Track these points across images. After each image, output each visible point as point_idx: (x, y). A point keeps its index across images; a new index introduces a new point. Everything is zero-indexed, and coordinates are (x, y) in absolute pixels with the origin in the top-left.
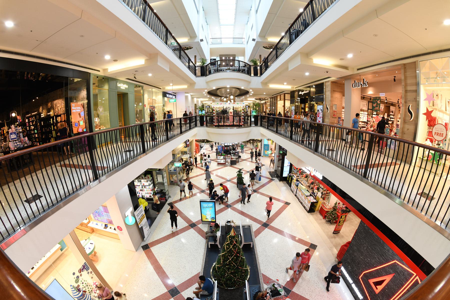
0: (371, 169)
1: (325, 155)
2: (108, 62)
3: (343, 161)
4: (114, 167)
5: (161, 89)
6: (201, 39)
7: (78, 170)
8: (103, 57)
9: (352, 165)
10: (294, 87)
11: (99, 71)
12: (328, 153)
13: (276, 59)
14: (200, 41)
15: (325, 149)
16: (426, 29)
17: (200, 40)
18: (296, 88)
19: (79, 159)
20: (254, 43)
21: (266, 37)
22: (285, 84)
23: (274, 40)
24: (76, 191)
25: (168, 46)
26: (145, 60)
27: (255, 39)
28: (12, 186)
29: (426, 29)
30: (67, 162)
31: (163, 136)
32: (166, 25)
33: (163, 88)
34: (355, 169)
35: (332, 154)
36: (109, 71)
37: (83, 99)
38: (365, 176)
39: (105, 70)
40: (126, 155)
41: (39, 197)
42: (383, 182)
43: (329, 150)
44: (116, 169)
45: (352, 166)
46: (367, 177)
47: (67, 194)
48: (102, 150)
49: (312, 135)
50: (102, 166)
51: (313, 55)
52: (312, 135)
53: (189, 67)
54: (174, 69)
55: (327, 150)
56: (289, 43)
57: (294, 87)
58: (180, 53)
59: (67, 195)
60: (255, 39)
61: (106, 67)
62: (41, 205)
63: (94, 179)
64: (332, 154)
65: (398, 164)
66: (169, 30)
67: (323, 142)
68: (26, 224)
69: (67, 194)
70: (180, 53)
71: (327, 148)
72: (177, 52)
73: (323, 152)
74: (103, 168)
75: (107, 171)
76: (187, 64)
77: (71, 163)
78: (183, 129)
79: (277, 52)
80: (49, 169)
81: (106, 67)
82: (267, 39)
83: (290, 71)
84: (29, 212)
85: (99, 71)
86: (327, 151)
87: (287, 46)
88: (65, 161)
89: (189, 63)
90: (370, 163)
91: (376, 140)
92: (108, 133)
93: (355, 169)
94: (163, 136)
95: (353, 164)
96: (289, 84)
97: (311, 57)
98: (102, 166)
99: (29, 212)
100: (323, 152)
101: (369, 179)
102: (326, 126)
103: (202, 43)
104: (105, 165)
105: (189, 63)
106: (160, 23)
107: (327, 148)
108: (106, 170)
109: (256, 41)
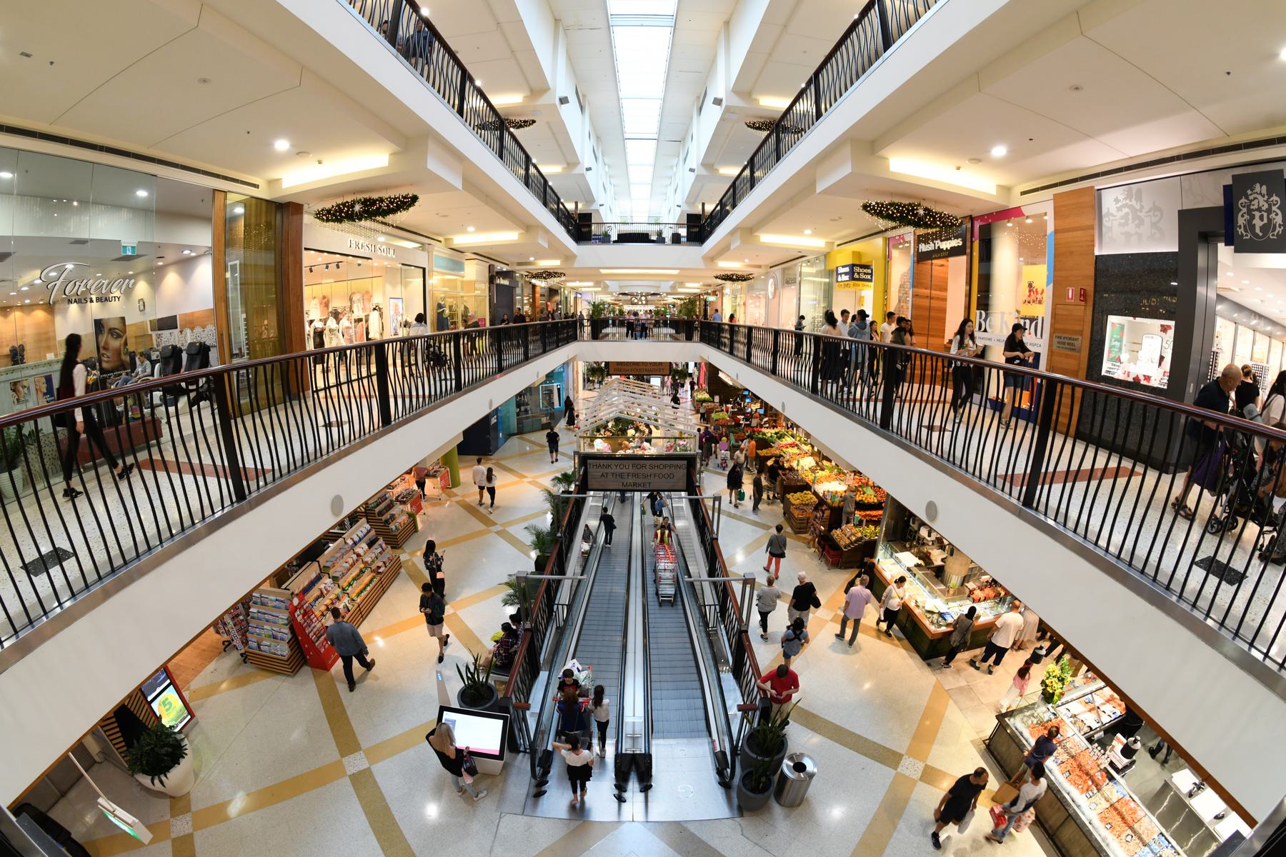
0: (1046, 487)
1: (908, 437)
2: (283, 159)
3: (959, 454)
4: (306, 460)
5: (440, 241)
6: (563, 95)
7: (175, 477)
8: (271, 145)
9: (998, 473)
10: (833, 243)
11: (256, 186)
12: (929, 436)
13: (777, 161)
14: (557, 102)
15: (920, 426)
16: (1228, 73)
17: (560, 99)
18: (1023, 193)
19: (274, 415)
20: (693, 175)
21: (754, 96)
22: (808, 232)
23: (776, 103)
24: (145, 553)
25: (439, 92)
26: (391, 154)
27: (721, 100)
28: (31, 505)
29: (1228, 73)
30: (143, 456)
31: (466, 370)
32: (458, 55)
33: (446, 239)
34: (1008, 485)
35: (940, 439)
36: (284, 186)
37: (1025, 323)
38: (1028, 501)
39: (273, 183)
40: (329, 435)
41: (58, 556)
42: (1042, 499)
43: (931, 428)
44: (312, 464)
45: (1000, 476)
46: (1035, 505)
47: (118, 562)
48: (303, 405)
49: (974, 412)
50: (259, 466)
51: (889, 144)
52: (974, 412)
53: (527, 181)
54: (477, 186)
55: (925, 427)
56: (814, 114)
57: (833, 243)
58: (501, 139)
59: (140, 550)
60: (721, 100)
61: (275, 174)
62: (106, 557)
63: (234, 499)
64: (940, 439)
65: (1138, 474)
66: (469, 74)
67: (912, 404)
68: (20, 634)
69: (118, 562)
70: (501, 139)
71: (925, 422)
72: (492, 136)
73: (914, 433)
74: (260, 472)
75: (272, 478)
76: (522, 172)
77: (156, 457)
78: (465, 376)
79: (778, 141)
80: (91, 480)
81: (275, 174)
82: (718, 170)
83: (820, 193)
84: (30, 598)
85: (256, 186)
86: (924, 431)
87: (854, 77)
88: (138, 455)
89: (527, 169)
90: (1043, 470)
91: (948, 370)
92: (261, 369)
93: (1008, 485)
94: (466, 370)
95: (1001, 471)
96: (816, 233)
97: (884, 153)
98: (259, 466)
99: (30, 598)
100: (914, 433)
101: (1042, 508)
102: (923, 356)
103: (589, 175)
104: (268, 466)
105: (527, 169)
106: (447, 55)
107: (925, 422)
108: (269, 477)
109: (724, 103)
